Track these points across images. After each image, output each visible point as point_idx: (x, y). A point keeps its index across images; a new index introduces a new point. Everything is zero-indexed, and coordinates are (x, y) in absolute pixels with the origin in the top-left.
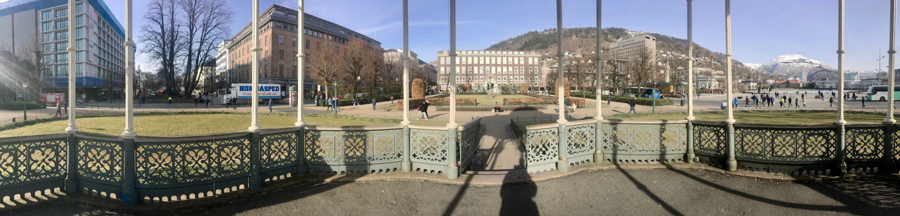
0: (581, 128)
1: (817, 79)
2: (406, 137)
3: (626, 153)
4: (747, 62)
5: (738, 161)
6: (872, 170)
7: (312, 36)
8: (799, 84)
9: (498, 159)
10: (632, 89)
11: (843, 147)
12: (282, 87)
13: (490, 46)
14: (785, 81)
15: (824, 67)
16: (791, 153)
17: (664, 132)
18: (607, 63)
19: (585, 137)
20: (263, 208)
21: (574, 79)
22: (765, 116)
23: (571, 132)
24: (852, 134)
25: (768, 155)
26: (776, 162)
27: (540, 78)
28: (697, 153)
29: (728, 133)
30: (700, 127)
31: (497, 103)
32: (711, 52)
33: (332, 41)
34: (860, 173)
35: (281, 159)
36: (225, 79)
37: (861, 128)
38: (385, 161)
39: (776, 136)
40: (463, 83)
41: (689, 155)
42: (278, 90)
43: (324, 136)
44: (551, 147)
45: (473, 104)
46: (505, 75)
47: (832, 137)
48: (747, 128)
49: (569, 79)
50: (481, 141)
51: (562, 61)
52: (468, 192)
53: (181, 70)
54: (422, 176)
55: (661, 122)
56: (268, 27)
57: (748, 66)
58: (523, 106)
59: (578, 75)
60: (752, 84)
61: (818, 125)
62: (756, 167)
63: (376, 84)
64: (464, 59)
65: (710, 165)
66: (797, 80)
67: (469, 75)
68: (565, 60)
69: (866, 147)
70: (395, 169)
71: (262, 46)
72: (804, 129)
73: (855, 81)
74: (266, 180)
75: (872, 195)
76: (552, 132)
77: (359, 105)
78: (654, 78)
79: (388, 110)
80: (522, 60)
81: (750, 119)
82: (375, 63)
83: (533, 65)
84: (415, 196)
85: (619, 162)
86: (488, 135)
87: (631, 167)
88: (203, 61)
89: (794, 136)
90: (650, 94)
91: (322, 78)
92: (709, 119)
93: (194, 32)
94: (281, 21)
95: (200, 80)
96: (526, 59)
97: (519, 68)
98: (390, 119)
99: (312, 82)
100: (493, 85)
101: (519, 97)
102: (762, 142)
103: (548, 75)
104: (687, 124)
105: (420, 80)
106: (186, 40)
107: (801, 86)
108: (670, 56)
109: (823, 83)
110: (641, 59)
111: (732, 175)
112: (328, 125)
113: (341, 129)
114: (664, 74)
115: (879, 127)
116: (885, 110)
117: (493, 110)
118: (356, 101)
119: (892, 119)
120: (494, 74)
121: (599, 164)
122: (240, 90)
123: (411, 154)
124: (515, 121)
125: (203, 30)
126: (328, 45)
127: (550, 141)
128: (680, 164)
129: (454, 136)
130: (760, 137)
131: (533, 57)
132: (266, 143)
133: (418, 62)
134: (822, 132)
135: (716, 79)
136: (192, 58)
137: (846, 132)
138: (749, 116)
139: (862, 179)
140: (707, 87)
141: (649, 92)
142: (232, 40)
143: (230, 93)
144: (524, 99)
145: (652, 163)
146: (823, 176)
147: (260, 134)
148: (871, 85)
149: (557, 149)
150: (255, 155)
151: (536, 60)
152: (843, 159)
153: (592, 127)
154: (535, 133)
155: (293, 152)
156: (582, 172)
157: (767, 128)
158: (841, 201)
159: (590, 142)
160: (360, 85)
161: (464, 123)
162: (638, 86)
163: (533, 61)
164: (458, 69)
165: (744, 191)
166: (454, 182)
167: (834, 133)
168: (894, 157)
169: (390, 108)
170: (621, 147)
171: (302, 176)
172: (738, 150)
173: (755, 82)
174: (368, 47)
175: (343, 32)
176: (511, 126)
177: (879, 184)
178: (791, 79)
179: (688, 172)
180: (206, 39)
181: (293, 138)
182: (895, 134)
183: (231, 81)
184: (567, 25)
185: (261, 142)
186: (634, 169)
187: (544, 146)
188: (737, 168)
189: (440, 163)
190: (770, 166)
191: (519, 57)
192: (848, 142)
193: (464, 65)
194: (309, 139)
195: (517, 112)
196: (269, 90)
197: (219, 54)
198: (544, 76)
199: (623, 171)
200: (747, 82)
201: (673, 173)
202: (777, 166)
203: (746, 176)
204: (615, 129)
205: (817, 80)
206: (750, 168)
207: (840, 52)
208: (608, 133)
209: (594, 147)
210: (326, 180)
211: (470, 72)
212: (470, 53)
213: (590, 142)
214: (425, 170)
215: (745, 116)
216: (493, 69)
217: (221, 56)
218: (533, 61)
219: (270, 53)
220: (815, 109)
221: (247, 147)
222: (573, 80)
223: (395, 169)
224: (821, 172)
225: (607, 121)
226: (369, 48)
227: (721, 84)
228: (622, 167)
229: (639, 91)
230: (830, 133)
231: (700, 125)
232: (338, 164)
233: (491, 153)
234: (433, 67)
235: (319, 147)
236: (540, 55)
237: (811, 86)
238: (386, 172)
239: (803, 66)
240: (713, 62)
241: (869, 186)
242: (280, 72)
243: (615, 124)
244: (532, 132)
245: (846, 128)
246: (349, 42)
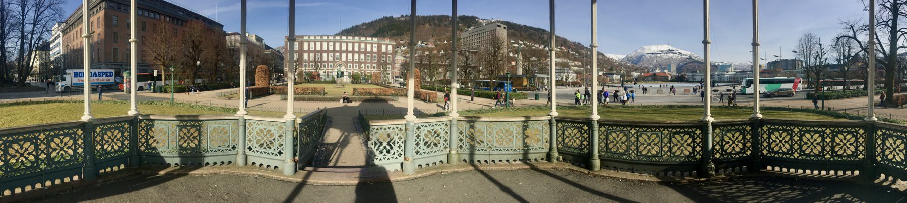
0: (433, 125)
1: (687, 71)
2: (241, 129)
3: (486, 153)
4: (609, 53)
5: (601, 160)
6: (741, 169)
7: (148, 17)
8: (668, 77)
9: (343, 154)
10: (484, 82)
11: (711, 146)
12: (116, 72)
13: (340, 31)
14: (651, 73)
15: (694, 58)
16: (657, 152)
17: (526, 130)
18: (458, 53)
19: (438, 135)
20: (98, 200)
21: (426, 71)
22: (629, 111)
23: (420, 130)
24: (720, 132)
25: (633, 154)
26: (641, 162)
27: (393, 68)
28: (561, 151)
29: (592, 131)
30: (564, 123)
31: (345, 93)
32: (569, 41)
33: (169, 22)
34: (729, 174)
35: (114, 149)
36: (60, 65)
37: (729, 125)
38: (220, 153)
39: (641, 134)
40: (311, 71)
41: (552, 153)
42: (112, 76)
43: (158, 126)
44: (397, 145)
45: (320, 94)
46: (356, 62)
47: (698, 136)
48: (612, 125)
49: (420, 70)
50: (326, 135)
51: (414, 50)
52: (305, 191)
53: (13, 55)
54: (258, 171)
55: (523, 119)
56: (100, 7)
57: (611, 57)
58: (373, 97)
59: (430, 67)
60: (614, 76)
61: (684, 123)
62: (614, 166)
63: (217, 70)
64: (312, 45)
65: (573, 164)
66: (665, 73)
67: (318, 63)
68: (417, 50)
69: (735, 144)
70: (230, 162)
71: (95, 28)
73: (729, 73)
74: (101, 172)
75: (739, 197)
76: (399, 128)
77: (198, 92)
78: (505, 71)
79: (229, 99)
80: (375, 47)
81: (613, 114)
82: (216, 47)
83: (386, 53)
84: (247, 192)
85: (476, 163)
86: (335, 127)
87: (491, 168)
88: (36, 45)
90: (502, 88)
91: (159, 63)
92: (567, 114)
93: (25, 12)
94: (115, 1)
95: (34, 66)
96: (379, 47)
97: (372, 56)
98: (230, 108)
99: (149, 66)
100: (342, 73)
101: (370, 88)
103: (402, 65)
104: (550, 121)
105: (264, 67)
106: (18, 20)
108: (523, 46)
109: (693, 76)
110: (492, 50)
111: (595, 175)
112: (163, 114)
113: (175, 118)
114: (515, 66)
115: (746, 123)
116: (752, 104)
117: (342, 101)
118: (195, 87)
119: (759, 114)
120: (344, 62)
121: (454, 165)
122: (75, 77)
123: (247, 147)
124: (363, 113)
125: (36, 10)
126: (165, 27)
127: (396, 138)
128: (543, 163)
129: (291, 129)
130: (625, 135)
131: (387, 45)
132: (100, 133)
133: (263, 47)
135: (574, 71)
136: (25, 41)
137: (713, 130)
138: (611, 112)
139: (731, 180)
140: (564, 80)
141: (502, 85)
142: (66, 22)
143: (64, 80)
144: (374, 89)
145: (514, 163)
146: (690, 178)
147: (93, 123)
148: (746, 78)
149: (403, 148)
150: (89, 146)
151: (390, 48)
152: (711, 159)
153: (446, 125)
154: (379, 128)
155: (126, 142)
156: (434, 174)
157: (632, 125)
159: (444, 141)
160: (199, 70)
161: (303, 115)
162: (490, 79)
163: (387, 48)
164: (306, 56)
165: (608, 193)
166: (291, 179)
167: (700, 132)
169: (231, 96)
170: (478, 147)
171: (136, 168)
172: (602, 149)
174: (208, 29)
175: (182, 13)
176: (358, 118)
177: (748, 184)
178: (658, 71)
179: (552, 172)
180: (39, 21)
181: (127, 128)
182: (762, 129)
183: (66, 66)
184: (420, 12)
185: (95, 132)
186: (495, 170)
187: (388, 144)
189: (276, 157)
190: (635, 166)
191: (372, 44)
193: (312, 51)
194: (143, 128)
195: (367, 104)
196: (103, 76)
197: (53, 38)
198: (397, 66)
199: (483, 173)
200: (609, 74)
201: (537, 173)
202: (641, 166)
203: (611, 177)
204: (472, 127)
206: (615, 168)
207: (706, 42)
208: (464, 132)
209: (448, 146)
210: (160, 173)
211: (319, 58)
212: (319, 38)
213: (444, 141)
214: (261, 165)
215: (606, 112)
216: (344, 55)
217: (56, 39)
218: (387, 48)
219: (103, 36)
220: (683, 104)
221: (80, 137)
222: (424, 71)
223: (230, 162)
224: (687, 173)
225: (462, 118)
226: (209, 31)
227: (579, 76)
228: (481, 168)
229: (492, 85)
230: (696, 132)
231: (564, 121)
232: (172, 156)
233: (336, 147)
234: (280, 53)
235: (152, 137)
236: (394, 43)
237: (680, 79)
238: (221, 165)
239: (672, 58)
240: (571, 52)
241: (738, 188)
242: (114, 57)
243: (473, 121)
244: (376, 127)
246: (188, 24)
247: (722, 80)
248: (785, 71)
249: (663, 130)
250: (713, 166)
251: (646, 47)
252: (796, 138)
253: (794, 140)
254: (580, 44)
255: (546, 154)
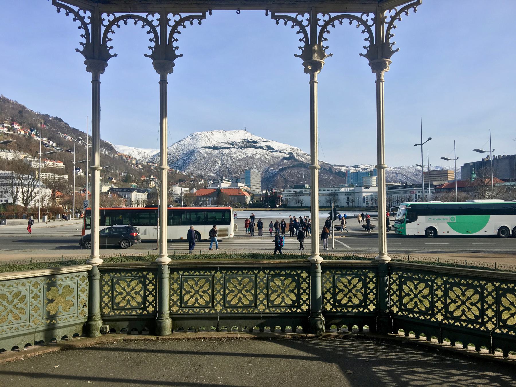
5: (173, 319)
8: (244, 197)
11: (319, 294)
14: (211, 189)
15: (299, 158)
28: (107, 318)
32: (31, 113)
41: (93, 323)
47: (304, 280)
57: (126, 153)
60: (134, 195)
72: (267, 268)
89: (254, 278)
102: (210, 288)
107: (248, 200)
109: (296, 195)
130: (208, 281)
134: (290, 273)
135: (45, 181)
137: (322, 273)
157: (217, 267)
158: (312, 353)
168: (390, 310)
173: (143, 192)
178: (225, 184)
182: (391, 277)
188: (172, 331)
192: (326, 287)
200: (122, 190)
205: (284, 187)
227: (58, 193)
239: (252, 157)
245: (322, 268)
247: (355, 204)
248: (507, 184)
249: (258, 273)
250: (323, 319)
251: (200, 134)
252: (439, 293)
253: (437, 295)
254: (61, 120)
255: (82, 326)
